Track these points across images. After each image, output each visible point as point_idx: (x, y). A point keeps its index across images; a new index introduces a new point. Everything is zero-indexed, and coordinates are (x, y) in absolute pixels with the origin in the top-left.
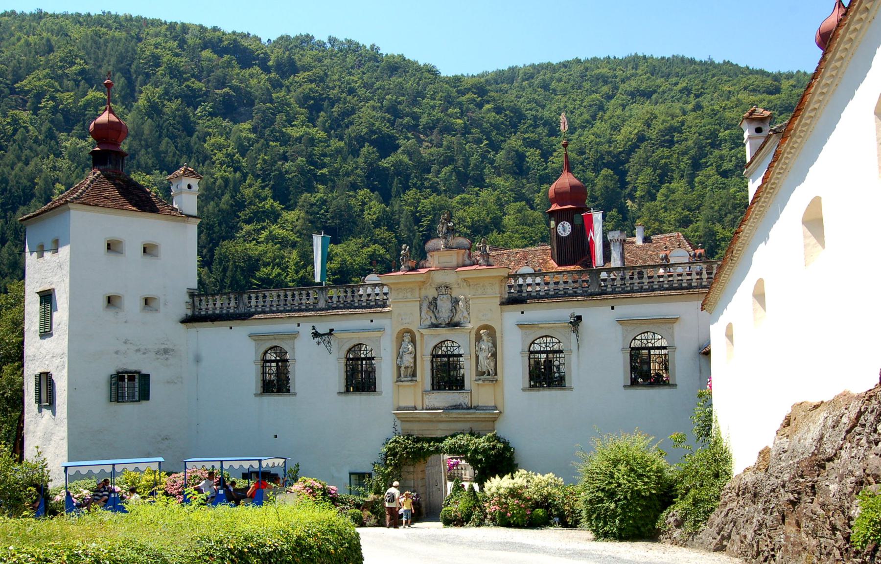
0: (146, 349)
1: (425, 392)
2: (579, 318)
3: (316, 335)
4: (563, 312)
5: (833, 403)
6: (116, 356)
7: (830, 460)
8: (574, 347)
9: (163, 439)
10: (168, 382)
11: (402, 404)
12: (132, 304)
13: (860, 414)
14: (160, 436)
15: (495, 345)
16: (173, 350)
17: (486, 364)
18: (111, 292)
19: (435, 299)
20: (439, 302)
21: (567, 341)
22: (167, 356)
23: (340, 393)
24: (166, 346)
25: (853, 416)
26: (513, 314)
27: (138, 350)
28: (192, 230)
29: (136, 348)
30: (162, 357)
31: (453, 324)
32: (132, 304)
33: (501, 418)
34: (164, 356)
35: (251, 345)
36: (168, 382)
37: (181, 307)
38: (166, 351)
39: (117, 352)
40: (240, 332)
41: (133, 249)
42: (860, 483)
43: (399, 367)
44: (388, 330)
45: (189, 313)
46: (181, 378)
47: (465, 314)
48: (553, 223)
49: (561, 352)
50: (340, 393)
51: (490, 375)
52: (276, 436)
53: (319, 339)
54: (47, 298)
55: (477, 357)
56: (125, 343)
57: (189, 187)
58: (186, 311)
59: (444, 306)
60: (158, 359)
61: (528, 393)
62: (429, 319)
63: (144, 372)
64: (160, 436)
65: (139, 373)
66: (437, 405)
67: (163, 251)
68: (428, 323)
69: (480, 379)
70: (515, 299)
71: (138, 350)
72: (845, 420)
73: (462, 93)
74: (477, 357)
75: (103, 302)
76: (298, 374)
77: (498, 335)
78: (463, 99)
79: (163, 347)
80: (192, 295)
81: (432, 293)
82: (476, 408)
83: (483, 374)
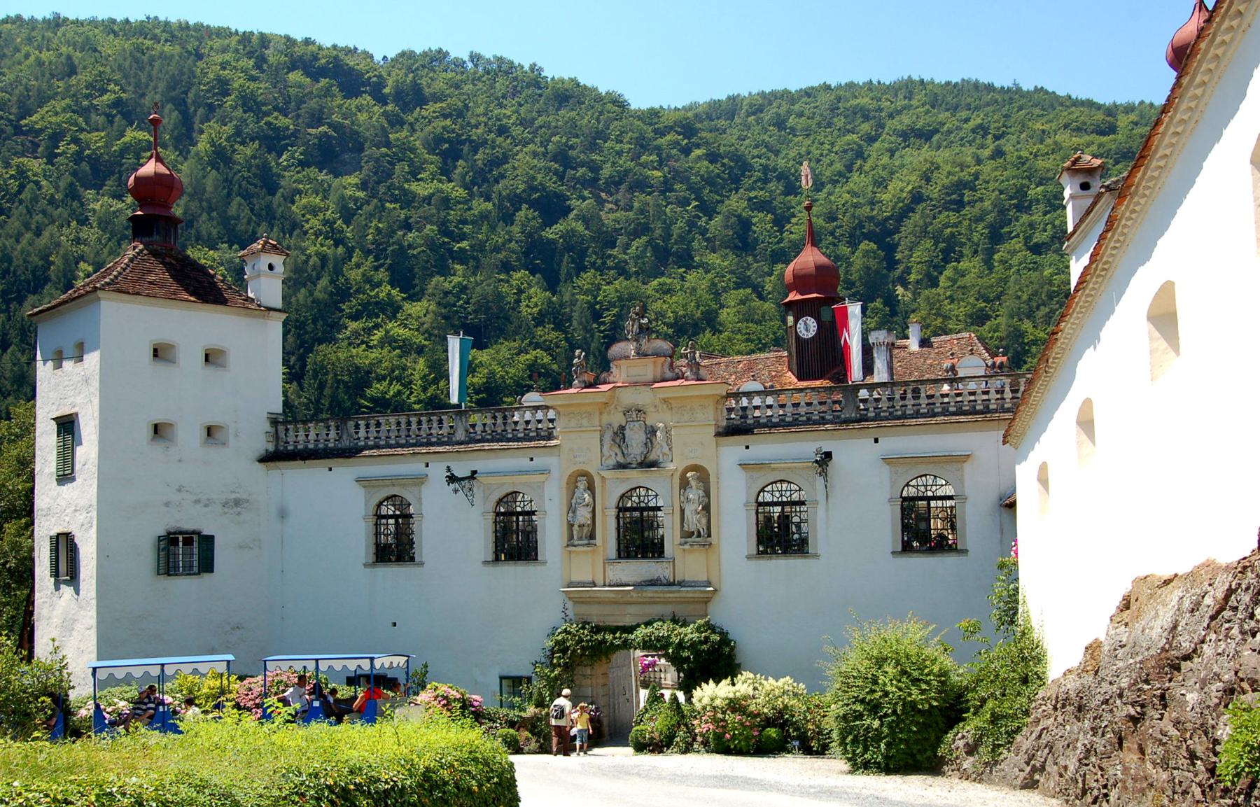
0: (208, 500)
1: (607, 561)
2: (828, 455)
3: (452, 479)
4: (805, 446)
5: (1192, 577)
6: (166, 509)
7: (1187, 658)
8: (821, 496)
9: (233, 629)
10: (241, 547)
11: (575, 578)
12: (188, 435)
13: (1230, 592)
14: (229, 624)
15: (707, 494)
16: (247, 501)
17: (694, 520)
18: (159, 418)
19: (622, 428)
20: (627, 433)
21: (811, 488)
22: (239, 509)
23: (486, 563)
24: (238, 495)
25: (1220, 595)
26: (734, 450)
27: (198, 501)
28: (274, 329)
29: (195, 498)
30: (232, 511)
31: (648, 464)
32: (188, 435)
33: (716, 599)
34: (235, 509)
35: (359, 493)
36: (241, 547)
37: (259, 439)
38: (237, 503)
39: (167, 504)
40: (344, 475)
41: (190, 356)
42: (1230, 691)
43: (571, 526)
44: (555, 473)
45: (271, 447)
46: (260, 540)
47: (666, 449)
48: (790, 319)
49: (802, 503)
50: (486, 563)
51: (701, 537)
52: (395, 624)
53: (456, 485)
54: (67, 426)
55: (682, 511)
56: (179, 490)
57: (271, 267)
58: (266, 446)
59: (636, 438)
60: (226, 513)
61: (754, 563)
62: (613, 457)
63: (206, 532)
64: (229, 624)
65: (198, 533)
66: (625, 579)
67: (233, 359)
68: (612, 462)
69: (686, 543)
70: (737, 429)
71: (198, 501)
72: (1208, 600)
73: (661, 133)
74: (682, 511)
75: (147, 432)
76: (427, 535)
77: (712, 479)
78: (663, 141)
79: (233, 496)
80: (274, 422)
81: (617, 419)
82: (681, 584)
83: (691, 534)
